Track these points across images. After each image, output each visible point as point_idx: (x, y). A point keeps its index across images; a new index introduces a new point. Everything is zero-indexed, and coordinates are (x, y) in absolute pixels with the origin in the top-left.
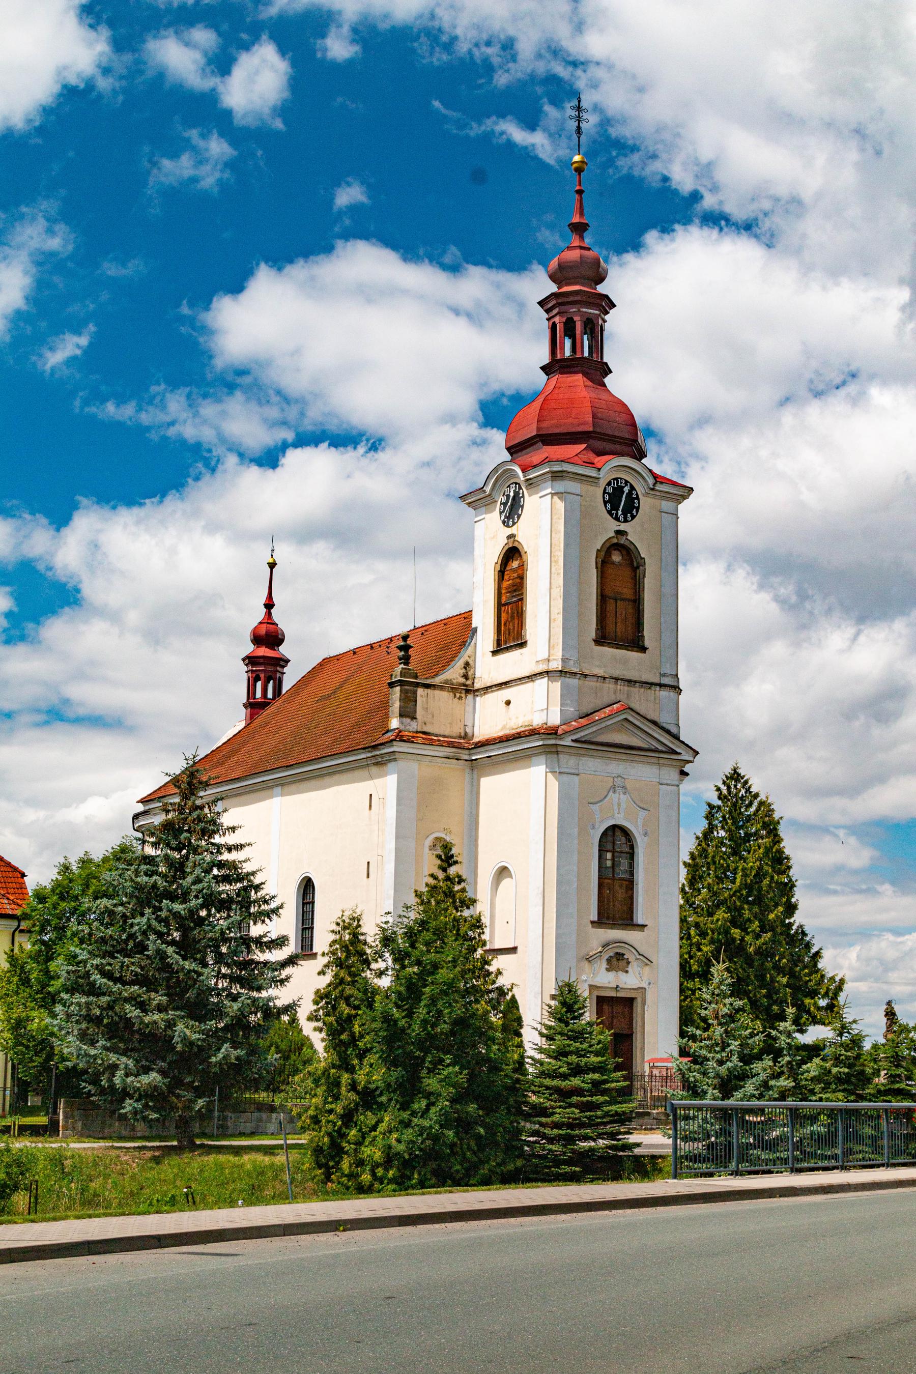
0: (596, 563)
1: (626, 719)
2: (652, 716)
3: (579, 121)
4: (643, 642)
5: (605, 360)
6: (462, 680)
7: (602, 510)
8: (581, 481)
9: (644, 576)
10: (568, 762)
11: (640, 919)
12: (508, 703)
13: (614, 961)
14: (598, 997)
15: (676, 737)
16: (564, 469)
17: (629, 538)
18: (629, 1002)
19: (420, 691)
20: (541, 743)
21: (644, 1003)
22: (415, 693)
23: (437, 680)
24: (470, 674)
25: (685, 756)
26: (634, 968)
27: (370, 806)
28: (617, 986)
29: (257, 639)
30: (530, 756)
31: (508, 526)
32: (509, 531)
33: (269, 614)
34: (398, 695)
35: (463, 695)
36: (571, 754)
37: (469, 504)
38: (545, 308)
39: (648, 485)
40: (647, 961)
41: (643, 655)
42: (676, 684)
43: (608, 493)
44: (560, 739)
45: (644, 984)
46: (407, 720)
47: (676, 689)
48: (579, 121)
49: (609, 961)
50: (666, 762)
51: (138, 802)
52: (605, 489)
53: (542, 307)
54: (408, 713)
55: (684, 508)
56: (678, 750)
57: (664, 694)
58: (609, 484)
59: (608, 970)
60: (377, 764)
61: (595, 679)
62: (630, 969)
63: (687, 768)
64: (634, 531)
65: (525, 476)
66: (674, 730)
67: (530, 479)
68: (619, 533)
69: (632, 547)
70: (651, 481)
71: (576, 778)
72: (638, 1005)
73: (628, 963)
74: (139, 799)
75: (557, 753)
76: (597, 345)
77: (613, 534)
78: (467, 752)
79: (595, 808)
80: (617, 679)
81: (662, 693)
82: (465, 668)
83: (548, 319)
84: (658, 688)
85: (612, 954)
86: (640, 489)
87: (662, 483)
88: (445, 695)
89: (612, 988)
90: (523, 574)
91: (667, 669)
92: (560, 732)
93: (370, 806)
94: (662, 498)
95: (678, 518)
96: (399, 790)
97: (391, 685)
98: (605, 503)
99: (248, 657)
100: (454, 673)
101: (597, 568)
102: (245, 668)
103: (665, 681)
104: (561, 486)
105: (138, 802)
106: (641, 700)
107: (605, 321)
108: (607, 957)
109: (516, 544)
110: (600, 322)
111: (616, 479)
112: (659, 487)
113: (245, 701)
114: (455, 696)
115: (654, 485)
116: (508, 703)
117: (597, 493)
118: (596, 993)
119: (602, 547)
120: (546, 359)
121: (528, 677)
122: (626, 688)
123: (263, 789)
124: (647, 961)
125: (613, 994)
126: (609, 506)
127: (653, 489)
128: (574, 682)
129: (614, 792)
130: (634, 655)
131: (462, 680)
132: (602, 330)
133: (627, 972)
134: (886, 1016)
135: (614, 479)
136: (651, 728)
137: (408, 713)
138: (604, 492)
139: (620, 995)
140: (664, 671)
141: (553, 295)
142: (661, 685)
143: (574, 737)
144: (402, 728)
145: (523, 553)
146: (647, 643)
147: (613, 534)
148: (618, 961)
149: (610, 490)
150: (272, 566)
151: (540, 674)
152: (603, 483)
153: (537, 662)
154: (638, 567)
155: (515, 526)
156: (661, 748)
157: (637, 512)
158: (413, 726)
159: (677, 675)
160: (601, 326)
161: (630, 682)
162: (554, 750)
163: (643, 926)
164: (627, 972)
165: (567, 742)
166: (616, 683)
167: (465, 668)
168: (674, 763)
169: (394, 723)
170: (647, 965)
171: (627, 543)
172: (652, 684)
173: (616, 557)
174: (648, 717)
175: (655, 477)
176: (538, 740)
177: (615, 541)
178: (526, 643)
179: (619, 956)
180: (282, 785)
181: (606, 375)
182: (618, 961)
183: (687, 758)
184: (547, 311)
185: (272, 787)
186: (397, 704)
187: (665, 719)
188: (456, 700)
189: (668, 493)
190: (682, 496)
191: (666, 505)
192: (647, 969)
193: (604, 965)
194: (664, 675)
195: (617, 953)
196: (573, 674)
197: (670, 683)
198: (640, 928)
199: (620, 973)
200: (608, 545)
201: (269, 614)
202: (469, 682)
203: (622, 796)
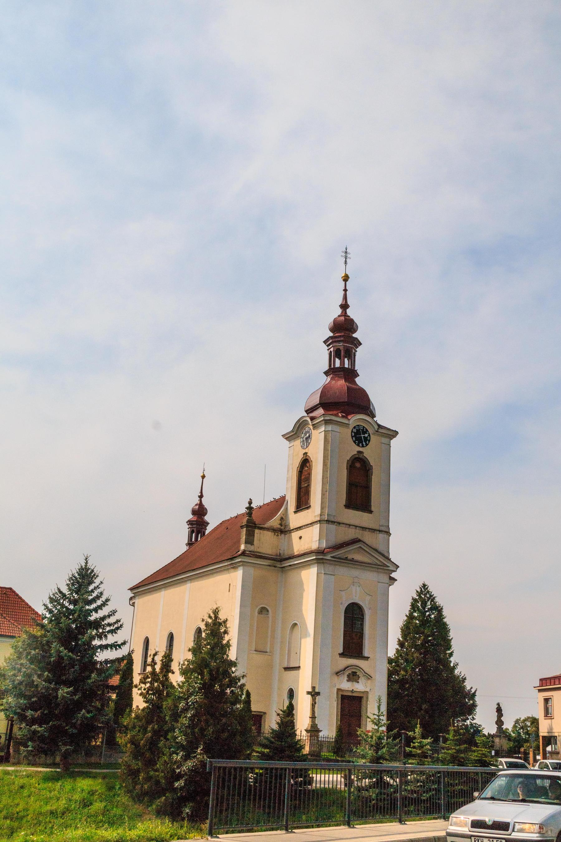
0: (347, 466)
1: (360, 547)
2: (374, 546)
3: (346, 258)
4: (371, 508)
5: (356, 369)
6: (279, 526)
7: (350, 440)
8: (340, 425)
9: (372, 475)
10: (330, 568)
11: (366, 653)
12: (300, 538)
13: (351, 676)
14: (342, 695)
15: (390, 560)
16: (331, 418)
17: (364, 455)
18: (359, 699)
19: (257, 531)
20: (315, 557)
21: (367, 698)
22: (254, 532)
23: (266, 526)
24: (283, 523)
25: (392, 568)
26: (362, 680)
27: (229, 590)
28: (353, 690)
29: (194, 512)
30: (309, 565)
31: (304, 449)
32: (304, 451)
33: (201, 501)
34: (245, 532)
35: (279, 534)
36: (331, 564)
37: (286, 438)
38: (327, 344)
39: (375, 429)
40: (369, 677)
41: (370, 515)
42: (387, 530)
43: (354, 432)
44: (324, 556)
45: (368, 690)
46: (249, 546)
47: (388, 533)
48: (346, 258)
49: (348, 676)
50: (380, 571)
51: (128, 590)
52: (352, 429)
53: (325, 344)
54: (250, 541)
55: (393, 442)
56: (388, 565)
57: (381, 536)
58: (355, 427)
59: (348, 681)
60: (233, 568)
61: (345, 525)
62: (360, 681)
63: (393, 575)
64: (368, 452)
65: (312, 423)
66: (386, 555)
67: (315, 424)
68: (360, 452)
69: (366, 460)
70: (376, 427)
71: (333, 577)
72: (364, 701)
73: (359, 677)
74: (129, 588)
75: (323, 563)
76: (353, 363)
77: (356, 453)
78: (279, 563)
79: (343, 593)
80: (356, 526)
81: (380, 535)
82: (281, 520)
83: (328, 350)
84: (378, 532)
85: (350, 672)
86: (371, 431)
87: (382, 428)
88: (269, 534)
89: (350, 691)
90: (310, 472)
91: (383, 522)
92: (325, 552)
93: (229, 590)
94: (382, 436)
95: (390, 447)
96: (243, 581)
97: (242, 527)
98: (352, 437)
99: (189, 521)
100: (274, 522)
101: (347, 469)
102: (188, 527)
103: (382, 528)
104: (329, 428)
105: (128, 590)
106: (368, 538)
107: (356, 351)
108: (347, 673)
109: (307, 457)
110: (353, 351)
111: (359, 425)
112: (380, 430)
113: (187, 542)
114: (275, 534)
115: (378, 429)
116: (300, 538)
117: (347, 433)
118: (341, 693)
119: (350, 459)
120: (327, 368)
121: (310, 524)
122: (361, 531)
123: (182, 582)
124: (369, 677)
125: (350, 694)
126: (354, 439)
127: (377, 431)
128: (333, 527)
129: (353, 585)
130: (366, 515)
131: (279, 526)
132: (355, 356)
133: (358, 682)
134: (474, 706)
135: (357, 425)
136: (373, 552)
137: (250, 541)
138: (352, 432)
139: (354, 694)
140: (381, 523)
141: (330, 338)
142: (380, 531)
143: (332, 555)
144: (246, 549)
145: (310, 461)
146: (373, 509)
147: (356, 453)
148: (353, 677)
149: (355, 430)
150: (203, 477)
151: (316, 522)
152: (351, 427)
153: (315, 516)
154: (369, 470)
155: (307, 449)
156: (379, 563)
157: (369, 443)
158: (251, 548)
159: (388, 526)
160: (354, 353)
161: (364, 529)
162: (322, 561)
163: (367, 658)
164: (358, 682)
165: (328, 557)
166: (356, 529)
167: (281, 520)
168: (386, 571)
169: (243, 547)
170: (369, 679)
171: (363, 458)
172: (375, 530)
173: (358, 465)
174: (373, 547)
175: (379, 426)
176: (313, 556)
177: (357, 456)
178: (310, 506)
179: (354, 674)
180: (190, 580)
181: (356, 377)
182: (353, 677)
183: (392, 569)
184: (328, 346)
185: (186, 581)
186: (244, 537)
187: (381, 548)
188: (275, 536)
189: (385, 433)
190: (392, 435)
191: (385, 440)
192: (369, 682)
193: (346, 678)
194: (382, 526)
195: (353, 672)
196: (333, 522)
197: (385, 530)
198: (366, 658)
199: (354, 683)
200: (353, 458)
201: (201, 501)
202: (282, 528)
203: (358, 588)
